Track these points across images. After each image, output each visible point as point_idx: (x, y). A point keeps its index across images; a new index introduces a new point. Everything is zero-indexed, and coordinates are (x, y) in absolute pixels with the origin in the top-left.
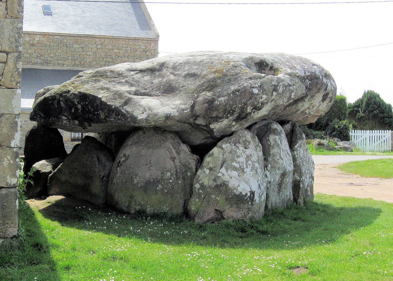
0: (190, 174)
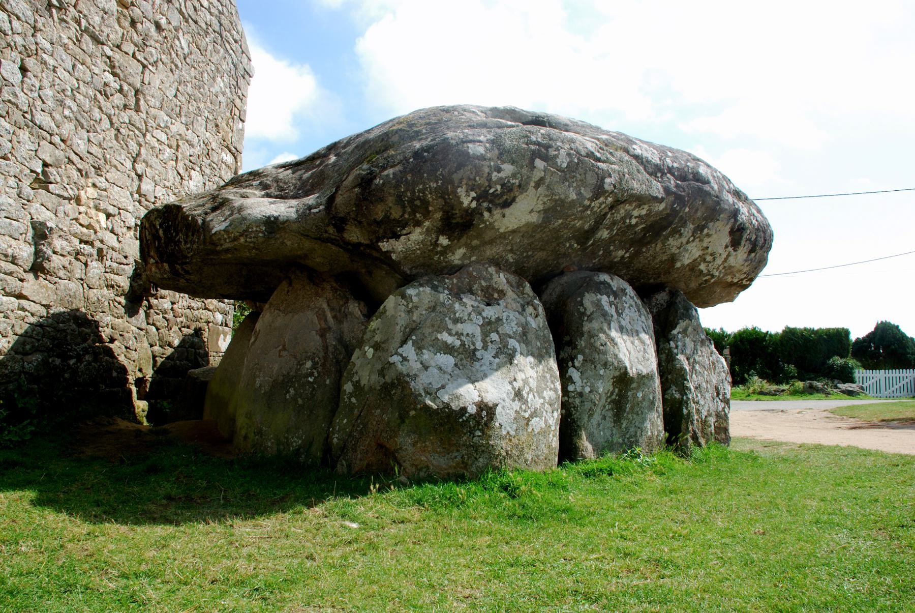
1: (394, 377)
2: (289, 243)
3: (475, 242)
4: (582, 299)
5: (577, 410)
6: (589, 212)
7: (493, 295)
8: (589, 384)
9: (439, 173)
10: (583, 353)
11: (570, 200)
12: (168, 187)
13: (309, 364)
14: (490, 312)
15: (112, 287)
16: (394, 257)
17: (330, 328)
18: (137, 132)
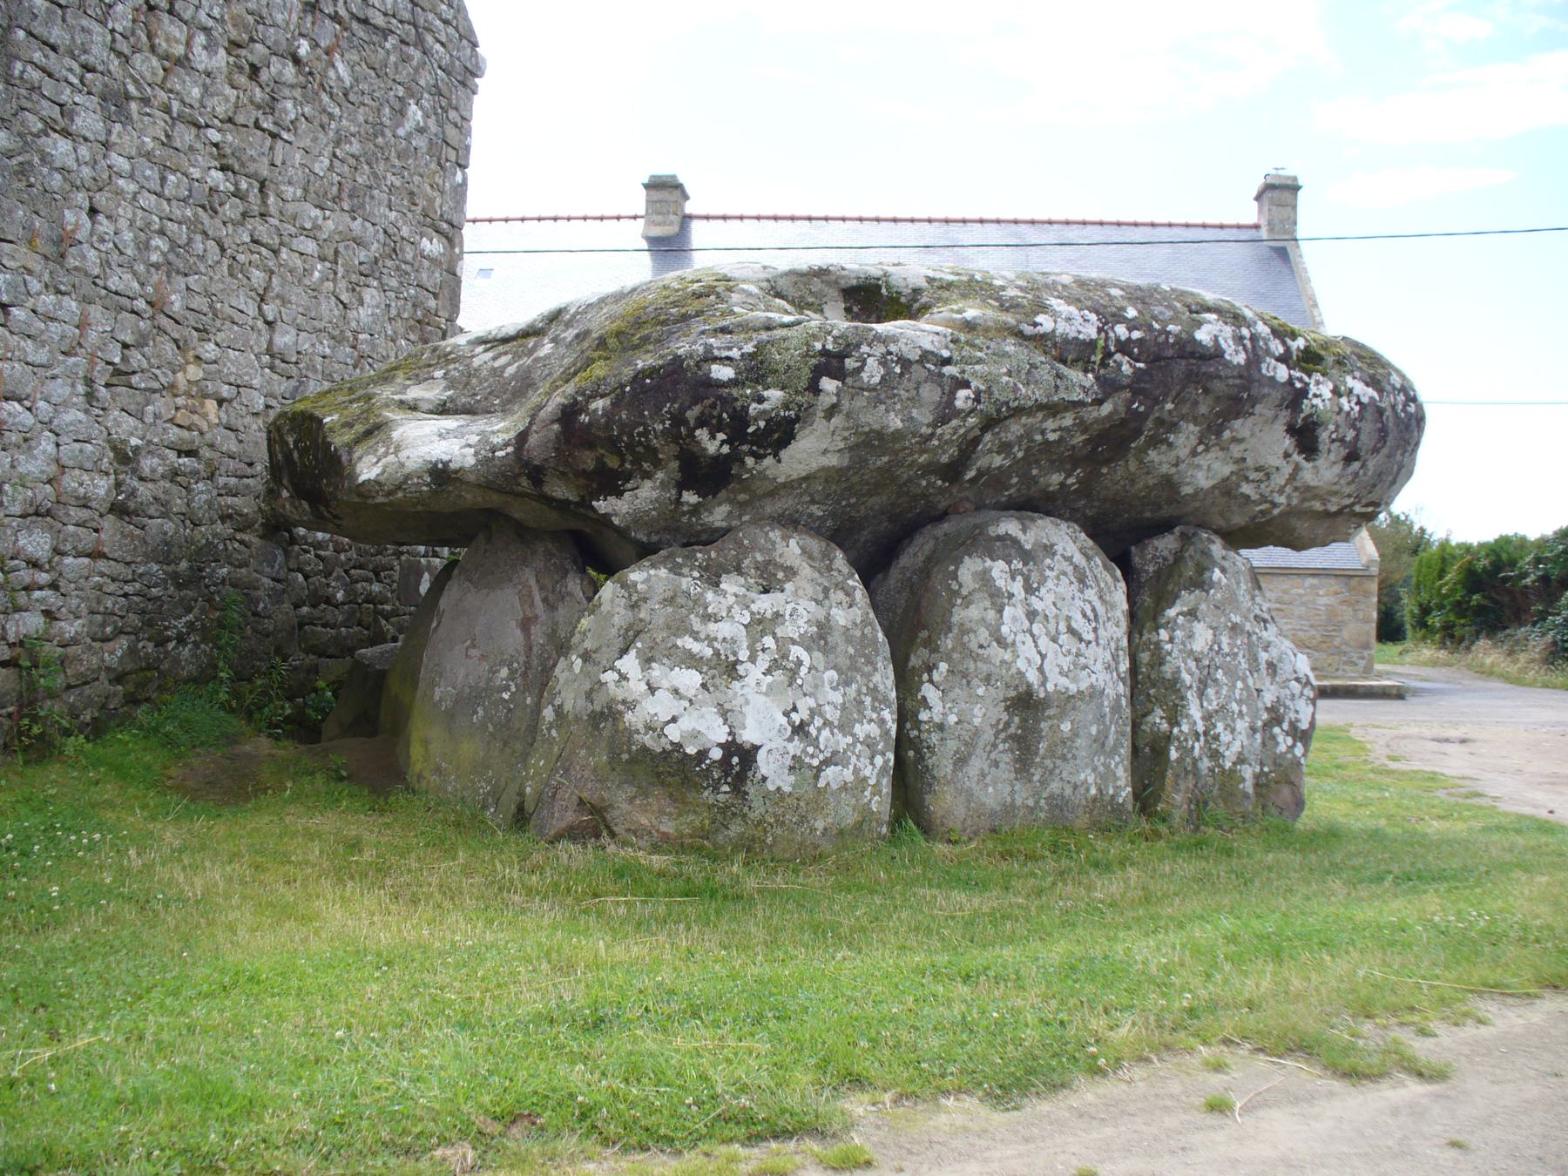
2: (468, 496)
3: (742, 497)
4: (957, 569)
5: (933, 753)
7: (775, 575)
10: (948, 659)
13: (504, 672)
14: (765, 604)
15: (230, 516)
16: (616, 521)
17: (536, 617)
18: (264, 251)
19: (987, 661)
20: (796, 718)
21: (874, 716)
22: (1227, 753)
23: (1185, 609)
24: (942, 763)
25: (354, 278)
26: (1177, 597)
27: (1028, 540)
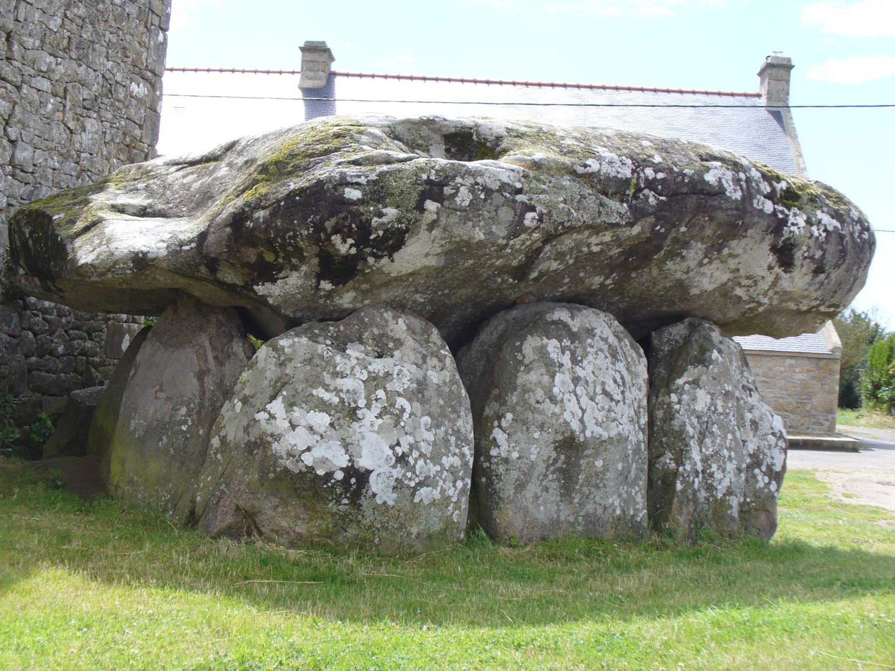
0: (596, 463)
1: (258, 437)
2: (161, 279)
3: (365, 286)
4: (522, 344)
5: (500, 480)
6: (509, 251)
7: (387, 345)
8: (517, 449)
9: (310, 220)
10: (513, 411)
11: (476, 240)
12: (52, 149)
13: (184, 410)
14: (379, 366)
16: (271, 301)
19: (542, 412)
20: (399, 450)
21: (457, 451)
22: (719, 487)
23: (691, 379)
24: (505, 487)
25: (79, 110)
26: (685, 370)
27: (575, 325)
